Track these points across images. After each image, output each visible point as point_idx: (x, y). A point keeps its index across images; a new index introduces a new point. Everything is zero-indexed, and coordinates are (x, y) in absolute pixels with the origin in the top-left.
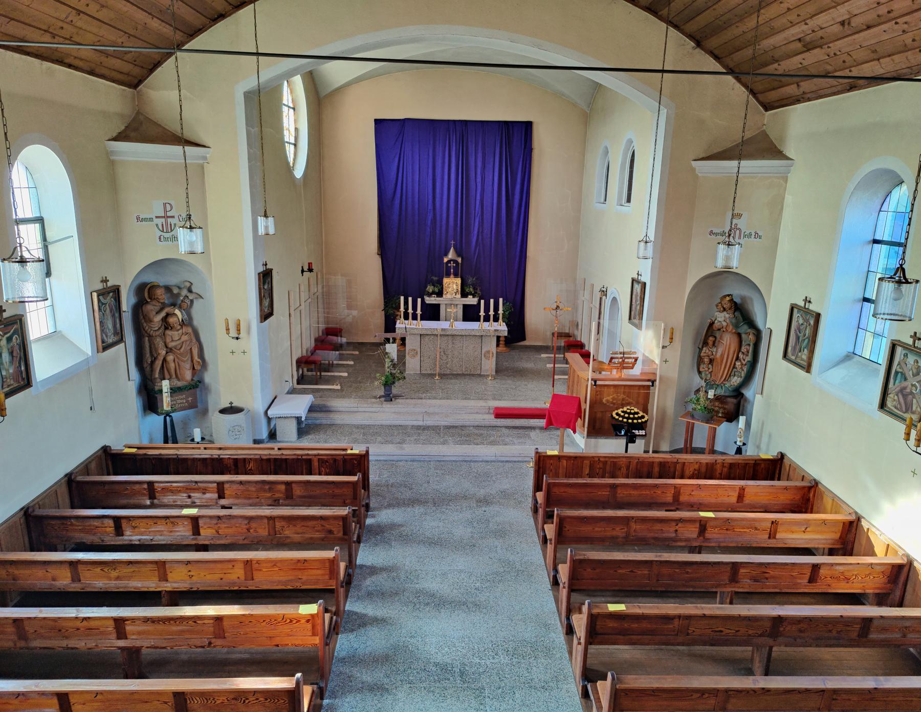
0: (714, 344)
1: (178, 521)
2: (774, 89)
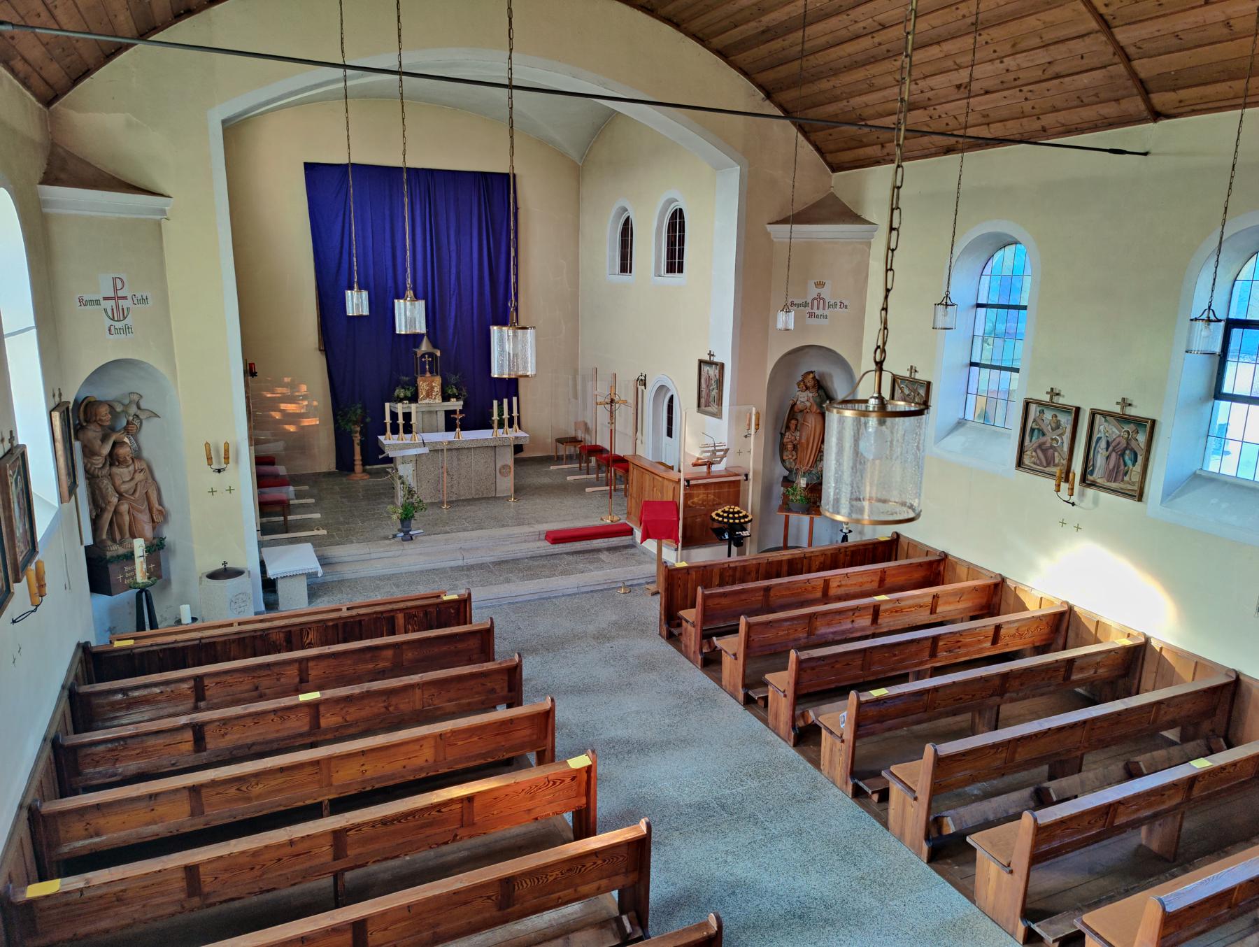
1: (288, 714)
2: (849, 149)
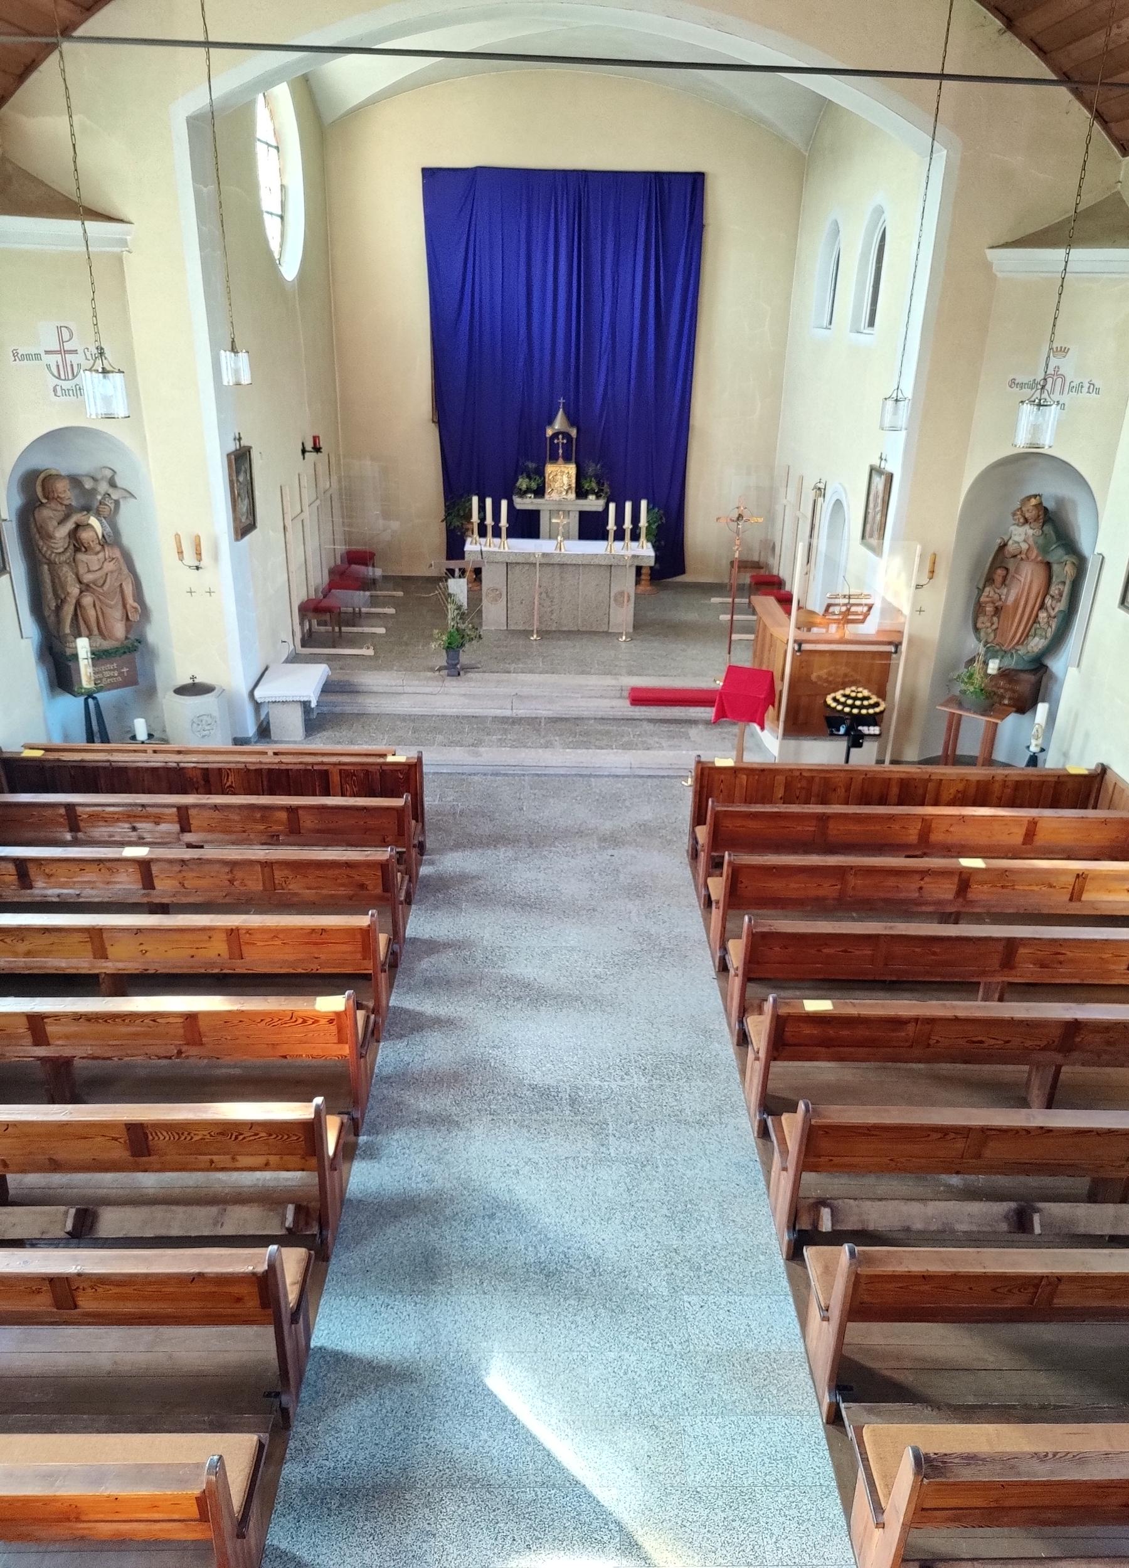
0: (1004, 582)
